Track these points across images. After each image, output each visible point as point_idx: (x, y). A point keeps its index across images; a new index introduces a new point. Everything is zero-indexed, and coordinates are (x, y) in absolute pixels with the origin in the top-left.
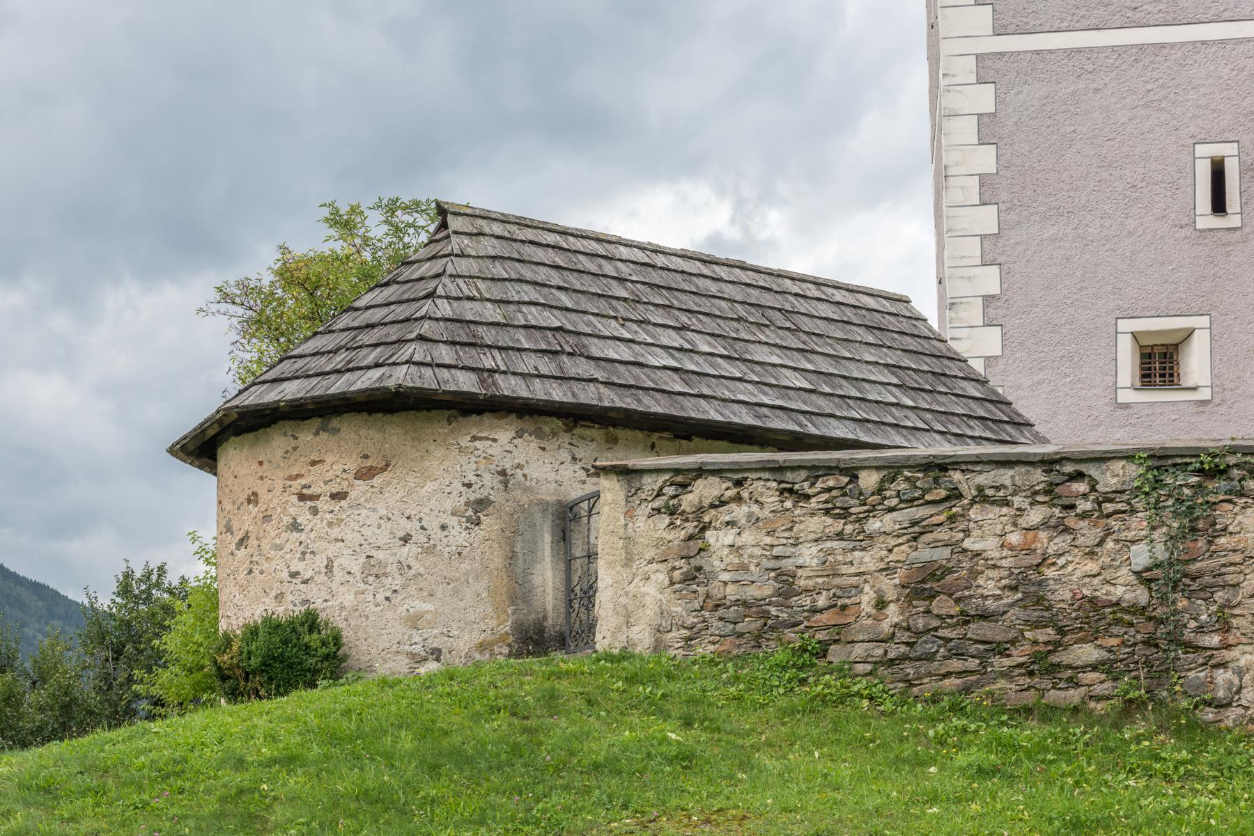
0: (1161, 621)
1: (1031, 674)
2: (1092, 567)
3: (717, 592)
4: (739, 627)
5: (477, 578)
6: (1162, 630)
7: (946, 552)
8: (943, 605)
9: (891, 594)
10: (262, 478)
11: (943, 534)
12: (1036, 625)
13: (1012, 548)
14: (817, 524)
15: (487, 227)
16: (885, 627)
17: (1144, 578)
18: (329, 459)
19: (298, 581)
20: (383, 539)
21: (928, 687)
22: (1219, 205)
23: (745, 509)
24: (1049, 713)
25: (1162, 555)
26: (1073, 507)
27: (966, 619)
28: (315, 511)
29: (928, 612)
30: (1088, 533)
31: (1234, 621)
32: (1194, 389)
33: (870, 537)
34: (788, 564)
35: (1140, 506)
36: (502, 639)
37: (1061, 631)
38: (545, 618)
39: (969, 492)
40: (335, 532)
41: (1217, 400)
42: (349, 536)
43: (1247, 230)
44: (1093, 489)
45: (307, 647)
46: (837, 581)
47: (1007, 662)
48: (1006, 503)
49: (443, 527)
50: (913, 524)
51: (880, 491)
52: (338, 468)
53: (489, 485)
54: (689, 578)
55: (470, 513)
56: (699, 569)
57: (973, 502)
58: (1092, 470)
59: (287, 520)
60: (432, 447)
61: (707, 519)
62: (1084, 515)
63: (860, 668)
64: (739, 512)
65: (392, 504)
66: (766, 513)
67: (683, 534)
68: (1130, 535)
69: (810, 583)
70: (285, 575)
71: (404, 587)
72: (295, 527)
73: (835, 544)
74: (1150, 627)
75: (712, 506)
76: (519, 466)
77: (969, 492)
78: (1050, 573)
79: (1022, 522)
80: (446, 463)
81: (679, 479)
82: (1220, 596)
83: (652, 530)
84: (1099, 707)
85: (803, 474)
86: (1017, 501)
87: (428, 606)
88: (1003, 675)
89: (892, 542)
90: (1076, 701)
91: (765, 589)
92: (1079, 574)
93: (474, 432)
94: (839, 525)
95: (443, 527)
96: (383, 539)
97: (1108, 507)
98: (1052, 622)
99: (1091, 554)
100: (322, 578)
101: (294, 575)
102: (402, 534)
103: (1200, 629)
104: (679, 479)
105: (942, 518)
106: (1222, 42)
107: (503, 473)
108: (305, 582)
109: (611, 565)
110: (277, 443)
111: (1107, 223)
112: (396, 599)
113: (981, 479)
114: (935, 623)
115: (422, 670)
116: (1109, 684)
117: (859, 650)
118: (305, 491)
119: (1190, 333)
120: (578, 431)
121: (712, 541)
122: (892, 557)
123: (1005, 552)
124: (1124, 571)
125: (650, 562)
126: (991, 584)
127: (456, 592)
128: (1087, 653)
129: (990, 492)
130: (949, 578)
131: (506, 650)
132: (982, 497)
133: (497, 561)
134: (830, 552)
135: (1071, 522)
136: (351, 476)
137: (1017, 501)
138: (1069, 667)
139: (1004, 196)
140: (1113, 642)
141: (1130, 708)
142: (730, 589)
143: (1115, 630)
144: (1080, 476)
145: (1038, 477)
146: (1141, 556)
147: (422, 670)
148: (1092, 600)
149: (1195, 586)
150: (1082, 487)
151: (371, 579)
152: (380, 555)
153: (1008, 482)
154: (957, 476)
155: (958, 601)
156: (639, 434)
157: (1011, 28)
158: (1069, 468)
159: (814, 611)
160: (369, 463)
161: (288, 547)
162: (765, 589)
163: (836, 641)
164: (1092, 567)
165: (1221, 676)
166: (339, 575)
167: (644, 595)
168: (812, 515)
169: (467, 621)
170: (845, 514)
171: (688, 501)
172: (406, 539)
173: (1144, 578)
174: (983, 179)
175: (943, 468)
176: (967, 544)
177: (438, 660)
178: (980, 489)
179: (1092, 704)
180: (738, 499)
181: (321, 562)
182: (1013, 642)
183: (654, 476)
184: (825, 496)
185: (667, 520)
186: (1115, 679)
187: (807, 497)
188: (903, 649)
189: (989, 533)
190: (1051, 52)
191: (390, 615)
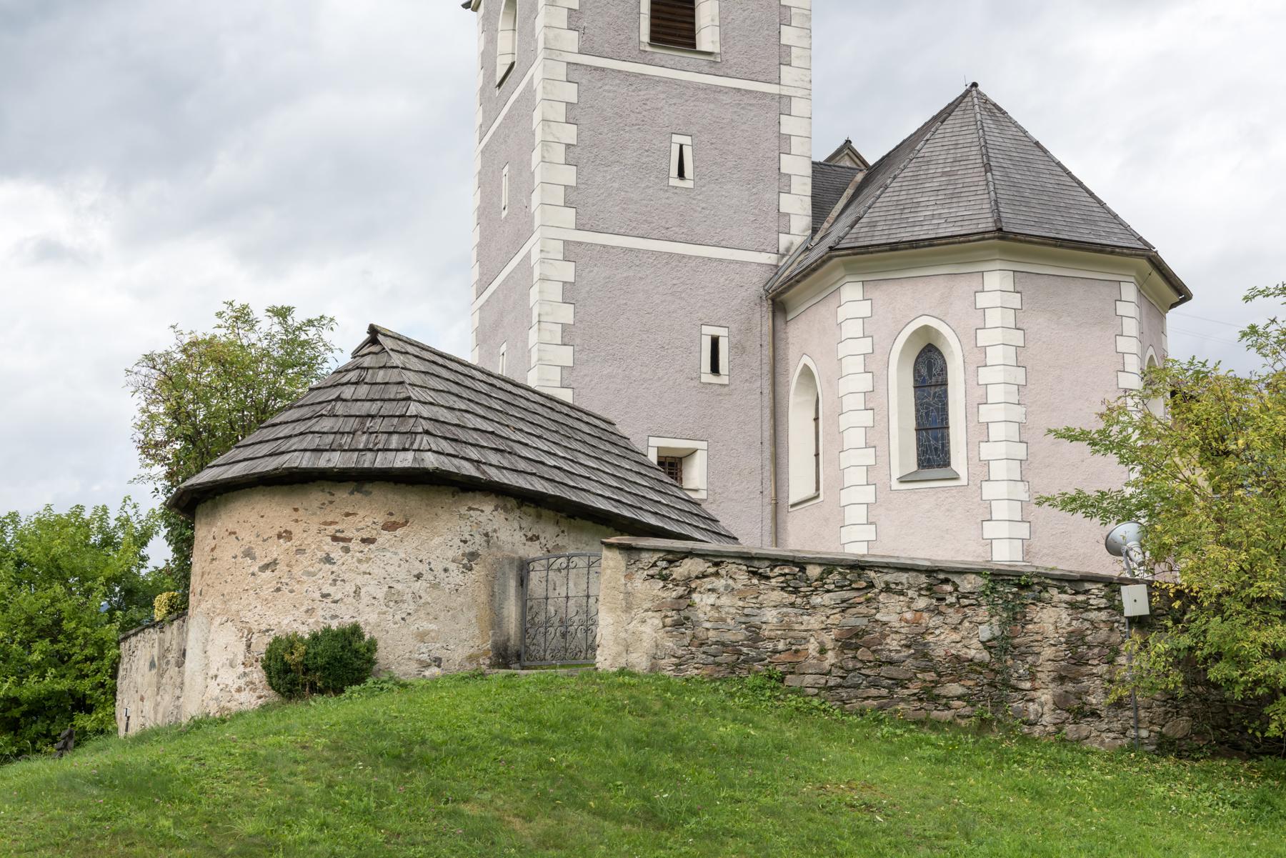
0: (998, 672)
1: (921, 700)
2: (956, 637)
3: (701, 633)
4: (718, 659)
5: (468, 609)
6: (999, 677)
7: (865, 621)
8: (861, 653)
9: (829, 645)
10: (297, 521)
11: (862, 609)
12: (924, 670)
13: (907, 622)
14: (777, 596)
15: (410, 349)
16: (826, 665)
17: (987, 645)
18: (361, 513)
19: (329, 600)
20: (402, 575)
21: (857, 704)
22: (715, 369)
23: (723, 582)
24: (936, 726)
25: (997, 633)
26: (944, 599)
27: (880, 664)
28: (347, 550)
29: (855, 658)
30: (954, 617)
31: (1039, 675)
32: (696, 490)
33: (814, 607)
34: (756, 621)
35: (984, 602)
36: (485, 654)
37: (939, 675)
38: (508, 640)
39: (880, 585)
40: (364, 567)
41: (710, 500)
42: (375, 571)
43: (732, 387)
44: (956, 590)
45: (357, 652)
46: (791, 634)
47: (906, 692)
48: (902, 593)
49: (446, 570)
50: (843, 602)
51: (821, 579)
52: (369, 521)
53: (478, 543)
54: (678, 624)
55: (465, 561)
56: (687, 618)
57: (881, 591)
58: (956, 579)
59: (320, 554)
60: (440, 512)
61: (693, 586)
62: (951, 605)
63: (810, 691)
64: (720, 583)
65: (409, 550)
66: (739, 586)
67: (674, 594)
68: (979, 619)
69: (773, 634)
70: (317, 595)
71: (416, 611)
72: (328, 560)
73: (789, 610)
74: (992, 675)
75: (697, 577)
76: (495, 531)
77: (880, 585)
78: (930, 638)
79: (914, 606)
80: (450, 525)
81: (670, 557)
82: (1030, 659)
83: (647, 589)
84: (963, 723)
85: (767, 563)
86: (910, 593)
87: (433, 627)
88: (903, 700)
89: (830, 612)
90: (950, 718)
91: (740, 635)
92: (948, 640)
93: (470, 504)
94: (792, 598)
95: (446, 570)
96: (402, 575)
97: (966, 602)
98: (934, 669)
99: (955, 629)
100: (351, 600)
101: (325, 596)
102: (416, 572)
103: (1019, 678)
104: (670, 557)
105: (862, 599)
106: (720, 260)
107: (486, 535)
108: (336, 602)
109: (611, 610)
110: (315, 498)
111: (645, 369)
112: (410, 620)
113: (888, 578)
114: (859, 665)
115: (427, 673)
116: (968, 708)
117: (809, 679)
118: (338, 534)
119: (693, 452)
120: (524, 508)
121: (697, 600)
122: (829, 621)
123: (903, 624)
124: (975, 640)
125: (646, 611)
126: (895, 643)
127: (454, 617)
128: (955, 689)
129: (893, 586)
130: (867, 637)
131: (488, 662)
132: (887, 589)
133: (483, 598)
134: (787, 615)
135: (943, 608)
136: (379, 527)
137: (910, 593)
138: (945, 697)
139: (578, 341)
140: (971, 683)
141: (984, 724)
142: (711, 633)
143: (972, 676)
144: (946, 581)
145: (923, 579)
146: (985, 632)
147: (427, 673)
148: (957, 657)
149: (1016, 652)
150: (949, 588)
151: (392, 604)
152: (399, 587)
153: (904, 581)
154: (872, 574)
155: (874, 652)
156: (552, 513)
157: (588, 227)
158: (942, 576)
159: (775, 652)
160: (393, 519)
161: (320, 575)
162: (740, 635)
163: (791, 673)
164: (956, 637)
165: (1032, 706)
166: (365, 599)
167: (642, 633)
168: (773, 590)
169: (463, 640)
170: (796, 591)
171: (680, 571)
172: (418, 577)
173: (987, 645)
174: (565, 327)
175: (863, 568)
176: (878, 617)
177: (439, 666)
178: (887, 584)
179: (959, 721)
180: (717, 574)
181: (350, 588)
182: (910, 680)
183: (651, 554)
184: (782, 579)
185: (661, 584)
186: (973, 706)
187: (768, 578)
188: (839, 680)
189: (892, 611)
190: (613, 247)
191: (404, 631)
